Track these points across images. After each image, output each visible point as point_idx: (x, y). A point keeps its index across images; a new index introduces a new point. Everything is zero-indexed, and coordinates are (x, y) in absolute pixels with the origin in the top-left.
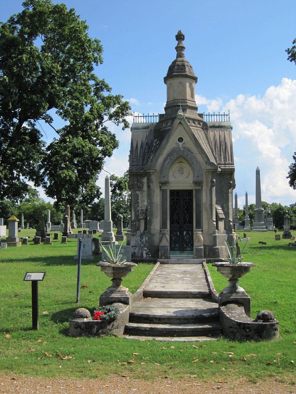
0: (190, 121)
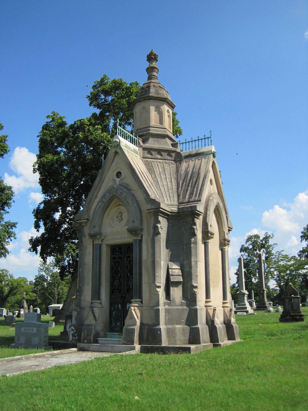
0: (153, 152)
